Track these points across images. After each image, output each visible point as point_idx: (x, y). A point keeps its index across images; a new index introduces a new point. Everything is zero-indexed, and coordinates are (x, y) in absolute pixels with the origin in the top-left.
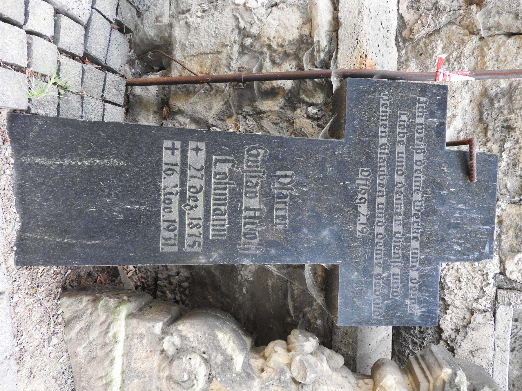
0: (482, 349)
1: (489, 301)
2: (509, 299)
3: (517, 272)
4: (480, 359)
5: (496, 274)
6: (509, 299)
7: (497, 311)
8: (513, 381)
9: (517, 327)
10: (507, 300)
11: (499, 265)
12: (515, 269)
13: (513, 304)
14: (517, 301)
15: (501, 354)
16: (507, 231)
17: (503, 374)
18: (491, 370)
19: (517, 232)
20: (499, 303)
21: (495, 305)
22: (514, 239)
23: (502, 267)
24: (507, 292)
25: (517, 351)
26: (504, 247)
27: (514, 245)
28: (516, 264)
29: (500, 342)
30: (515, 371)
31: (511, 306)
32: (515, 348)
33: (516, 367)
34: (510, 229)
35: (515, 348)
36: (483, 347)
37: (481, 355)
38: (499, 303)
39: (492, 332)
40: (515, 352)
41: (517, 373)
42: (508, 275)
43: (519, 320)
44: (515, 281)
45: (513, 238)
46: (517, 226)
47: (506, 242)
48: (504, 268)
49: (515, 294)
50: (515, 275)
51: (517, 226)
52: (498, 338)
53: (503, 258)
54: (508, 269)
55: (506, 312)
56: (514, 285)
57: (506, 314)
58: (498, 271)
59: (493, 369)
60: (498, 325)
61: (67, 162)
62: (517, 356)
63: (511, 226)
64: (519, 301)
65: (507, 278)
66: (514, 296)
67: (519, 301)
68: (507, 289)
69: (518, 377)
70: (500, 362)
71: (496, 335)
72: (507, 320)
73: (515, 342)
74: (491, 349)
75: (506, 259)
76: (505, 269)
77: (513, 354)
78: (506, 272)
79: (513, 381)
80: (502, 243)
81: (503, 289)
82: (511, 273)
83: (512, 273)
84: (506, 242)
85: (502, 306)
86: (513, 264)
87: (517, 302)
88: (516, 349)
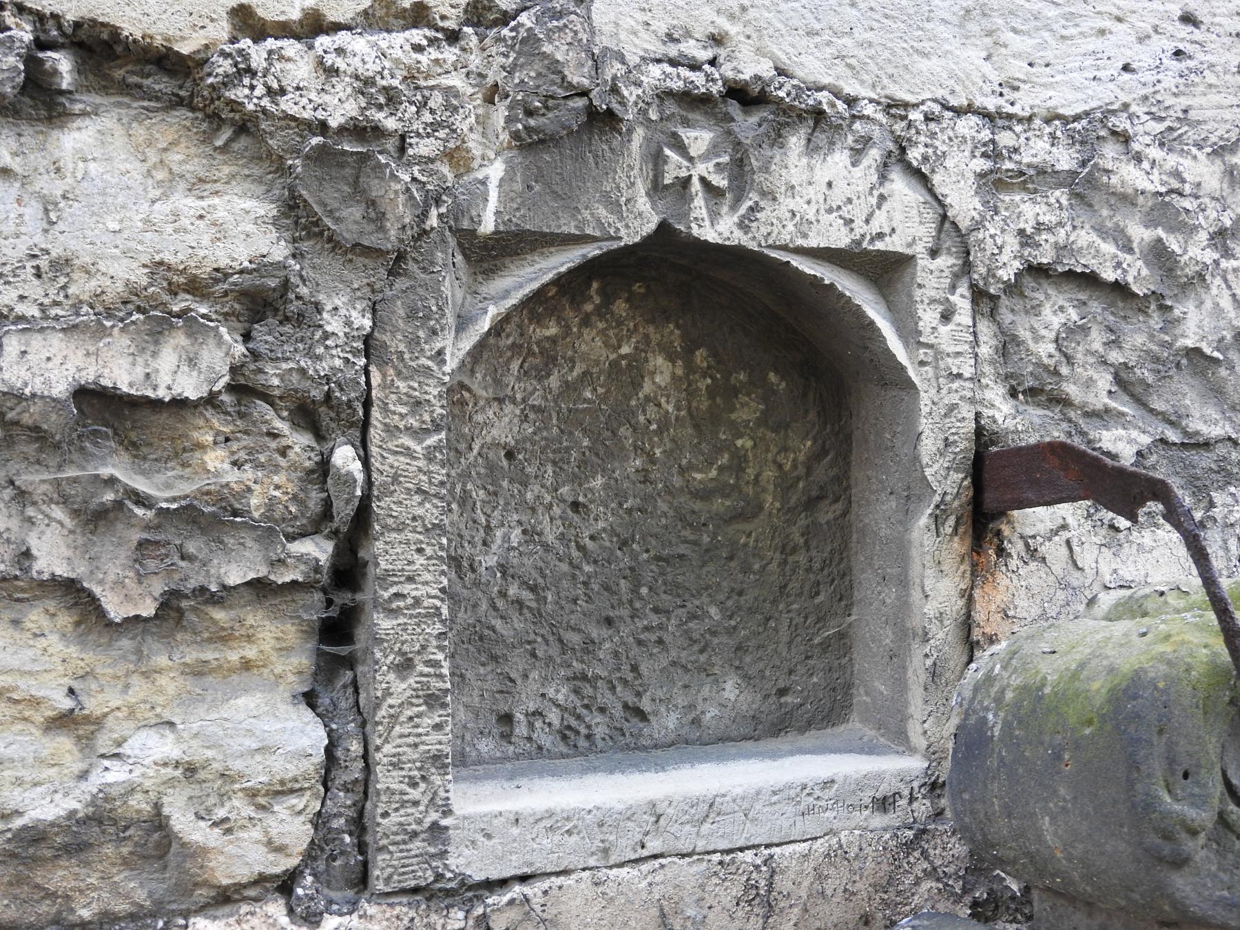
0: (663, 915)
1: (434, 917)
2: (415, 834)
3: (270, 821)
4: (711, 915)
5: (291, 912)
6: (415, 834)
7: (479, 877)
8: (766, 697)
9: (538, 713)
10: (417, 846)
11: (245, 908)
12: (256, 833)
13: (434, 816)
14: (416, 803)
15: (674, 828)
16: (52, 895)
17: (758, 806)
18: (748, 856)
19: (49, 853)
20: (439, 877)
21: (449, 893)
22: (92, 855)
23: (251, 893)
24: (381, 849)
25: (639, 694)
26: (141, 896)
27: (125, 850)
28: (229, 831)
29: (623, 842)
30: (726, 694)
31: (444, 822)
32: (626, 706)
33: (706, 691)
34: (38, 886)
35: (626, 706)
36: (655, 912)
37: (690, 912)
38: (439, 877)
39: (575, 884)
40: (646, 704)
41: (729, 685)
42: (294, 861)
43: (504, 708)
44: (319, 820)
45: (87, 864)
46: (13, 855)
47: (115, 890)
48: (255, 883)
49: (385, 815)
50: (286, 828)
51: (13, 855)
52: (606, 852)
53: (202, 894)
54: (258, 869)
55: (480, 838)
56: (338, 823)
57: (489, 836)
58: (276, 909)
59: (741, 850)
60: (541, 863)
61: (71, 472)
62: (660, 694)
63: (19, 881)
64: (414, 794)
65: (310, 856)
66: (395, 818)
67: (414, 794)
68: (362, 847)
69: (747, 678)
70: (706, 828)
71: (592, 862)
72: (515, 831)
73: (602, 710)
74: (659, 878)
75: (206, 884)
76: (261, 880)
77: (656, 713)
78: (278, 870)
79: (766, 697)
80: (121, 907)
81: (365, 864)
82: (280, 849)
83: (278, 842)
84: (115, 890)
85: (452, 861)
86: (230, 849)
87: (425, 801)
88: (631, 699)
